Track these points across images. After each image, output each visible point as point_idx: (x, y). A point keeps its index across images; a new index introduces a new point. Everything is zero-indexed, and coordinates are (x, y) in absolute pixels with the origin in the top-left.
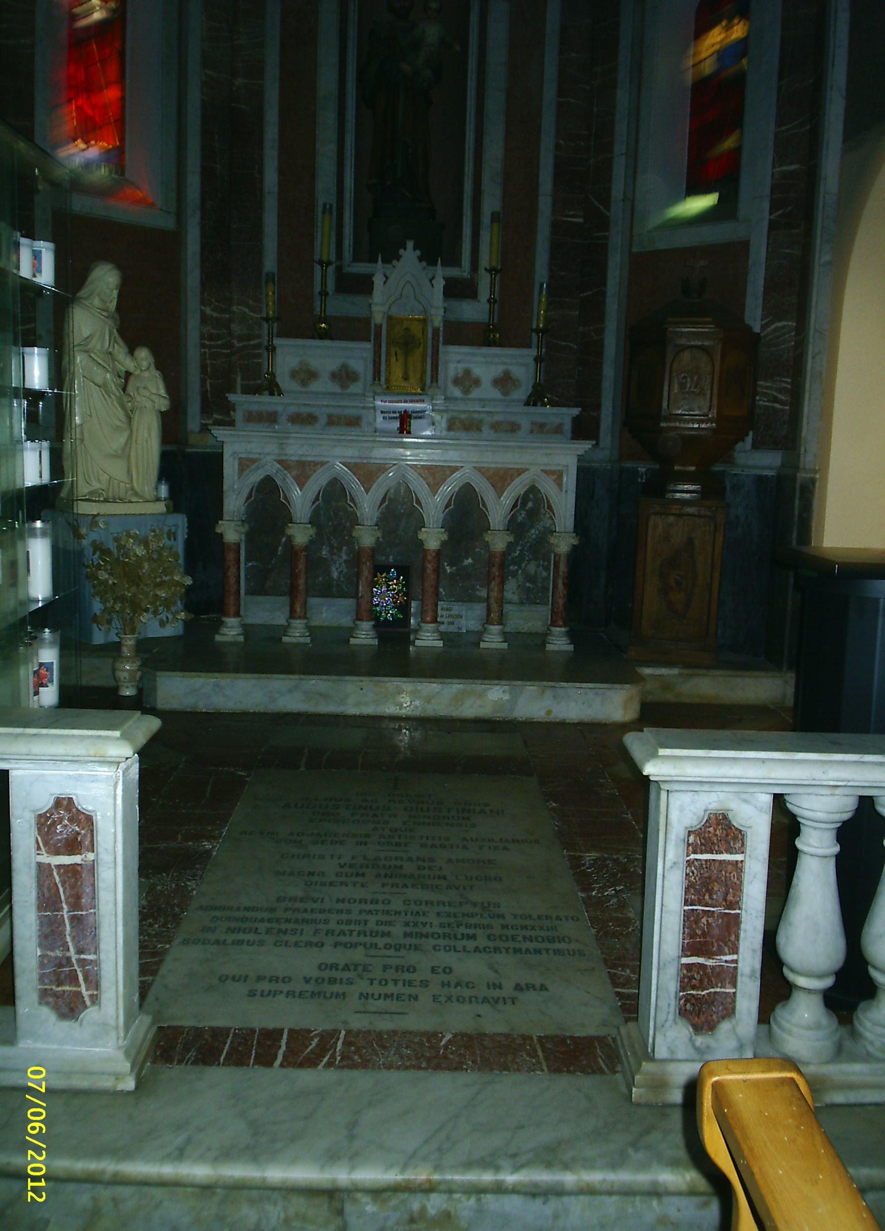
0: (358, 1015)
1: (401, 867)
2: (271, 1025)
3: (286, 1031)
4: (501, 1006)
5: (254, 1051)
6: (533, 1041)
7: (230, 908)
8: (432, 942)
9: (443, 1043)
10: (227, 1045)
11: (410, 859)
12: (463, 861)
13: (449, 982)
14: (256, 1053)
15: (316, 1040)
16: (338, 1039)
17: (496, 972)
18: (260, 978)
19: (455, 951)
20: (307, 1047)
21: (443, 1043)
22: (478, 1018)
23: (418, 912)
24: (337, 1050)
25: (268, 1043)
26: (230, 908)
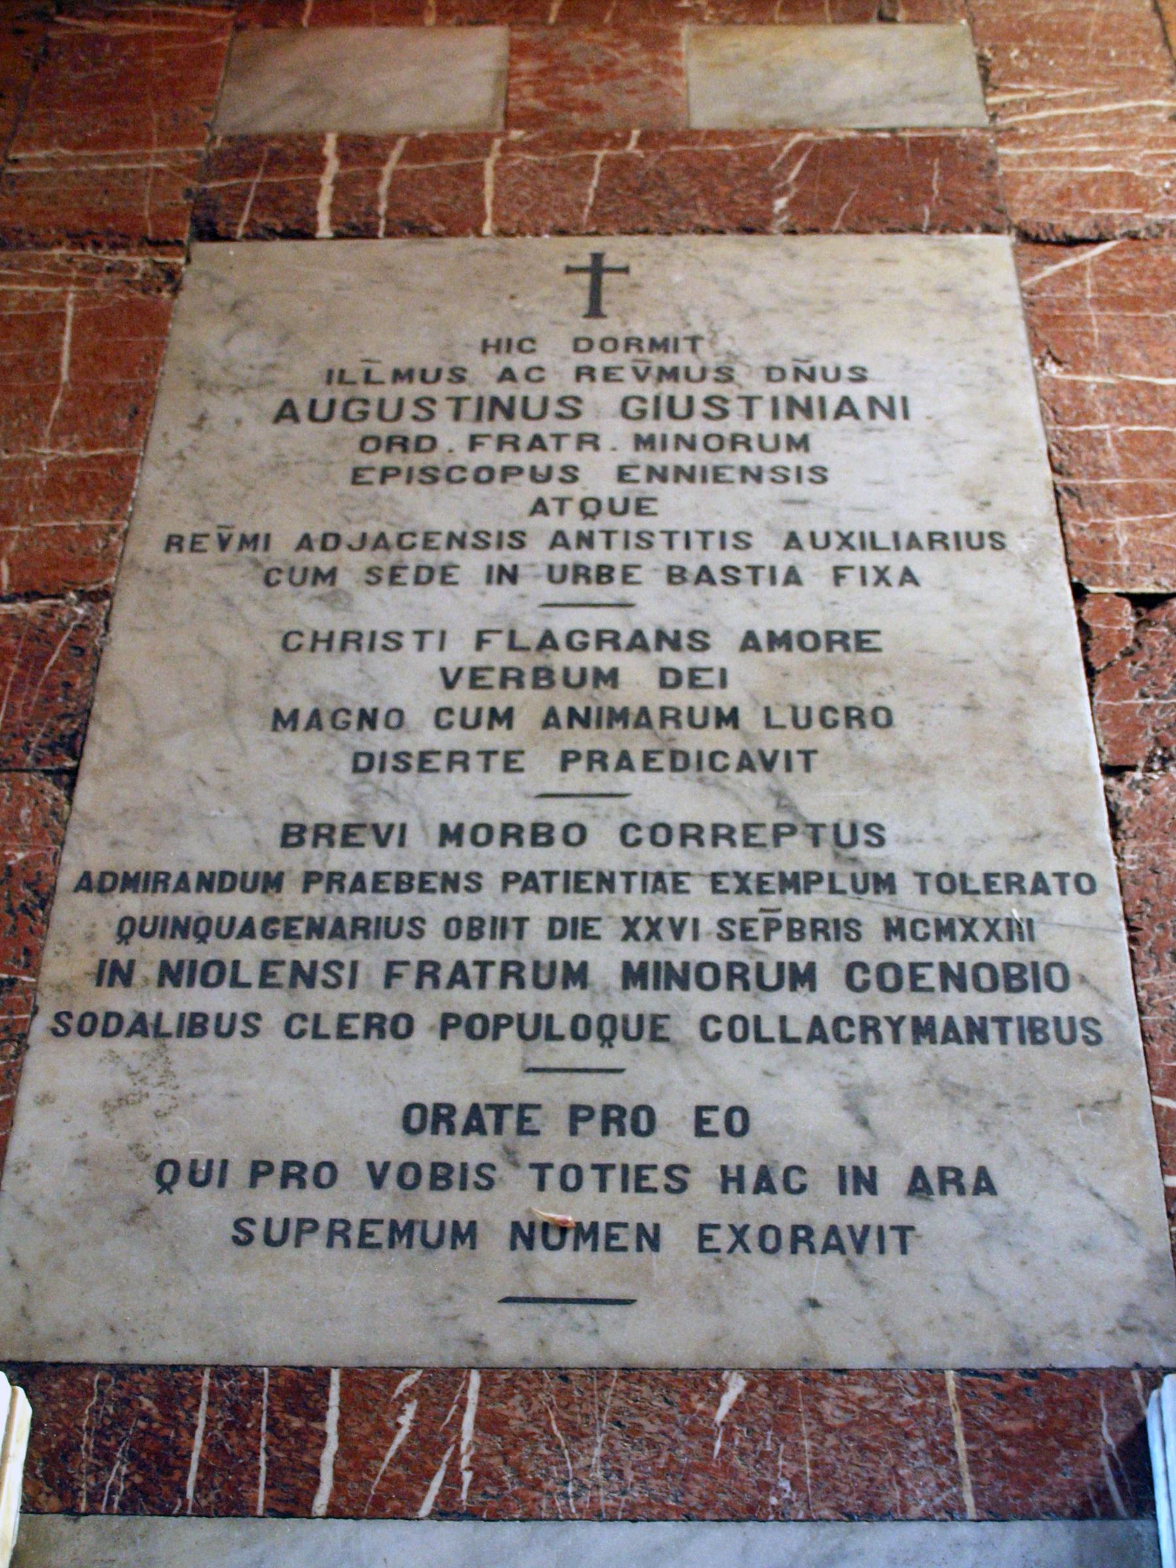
0: (512, 1310)
1: (612, 677)
2: (301, 1356)
3: (335, 1376)
4: (872, 1263)
5: (263, 1457)
6: (946, 1397)
7: (154, 881)
8: (699, 1002)
9: (721, 1414)
10: (199, 1433)
11: (638, 642)
12: (780, 641)
13: (484, 351)
14: (269, 1463)
15: (410, 1410)
16: (462, 1407)
17: (864, 1123)
18: (259, 1170)
19: (965, 891)
20: (390, 1436)
21: (721, 1414)
22: (810, 1314)
23: (677, 934)
24: (463, 1447)
25: (297, 1423)
26: (154, 881)
